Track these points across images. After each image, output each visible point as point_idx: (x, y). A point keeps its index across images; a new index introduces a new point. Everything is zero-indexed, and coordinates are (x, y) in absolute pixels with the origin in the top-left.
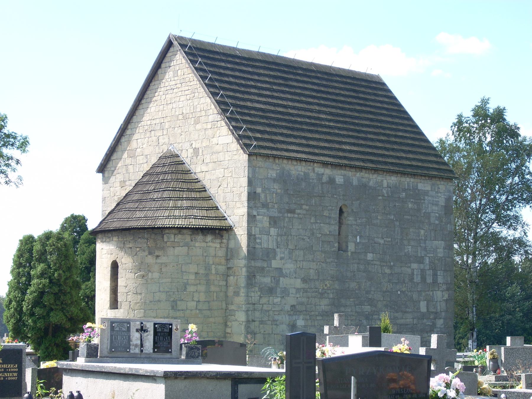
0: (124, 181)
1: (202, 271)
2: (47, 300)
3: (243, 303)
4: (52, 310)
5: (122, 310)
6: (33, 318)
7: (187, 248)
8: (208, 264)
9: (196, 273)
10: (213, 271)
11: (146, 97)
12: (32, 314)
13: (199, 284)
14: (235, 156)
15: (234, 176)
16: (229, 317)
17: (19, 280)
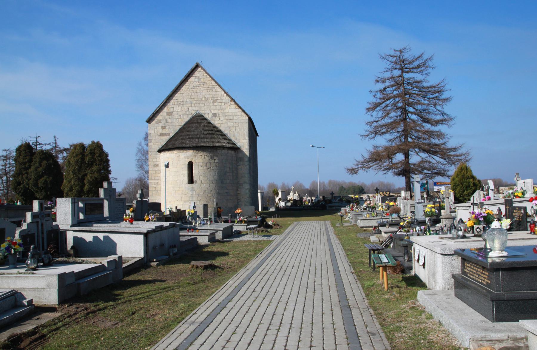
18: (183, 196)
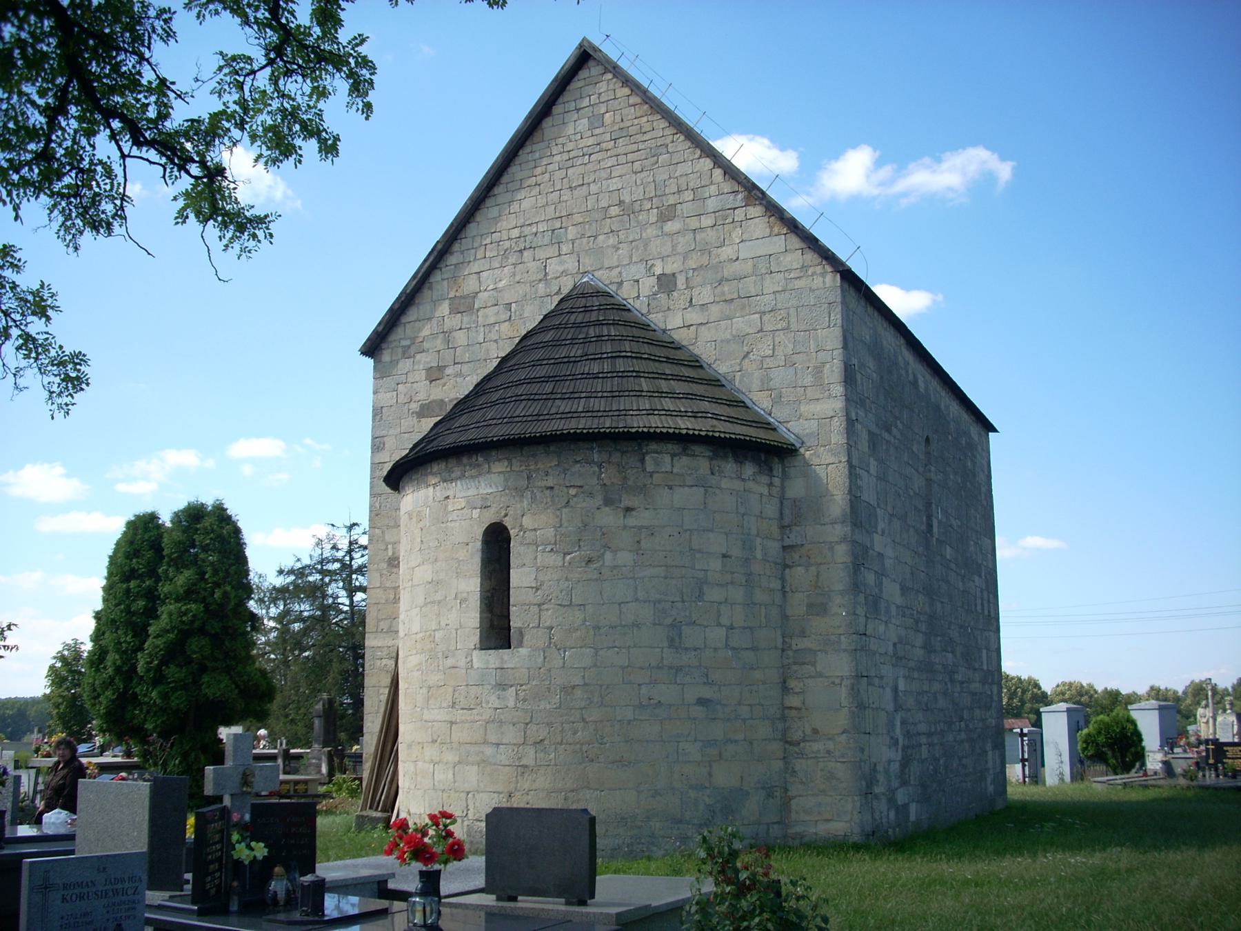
0: (441, 368)
1: (736, 552)
2: (197, 647)
3: (841, 631)
4: (203, 669)
5: (523, 651)
6: (161, 688)
7: (702, 489)
8: (749, 534)
9: (724, 556)
10: (759, 555)
11: (505, 179)
12: (158, 679)
13: (732, 583)
14: (796, 282)
15: (794, 326)
16: (795, 667)
17: (128, 606)
18: (459, 715)
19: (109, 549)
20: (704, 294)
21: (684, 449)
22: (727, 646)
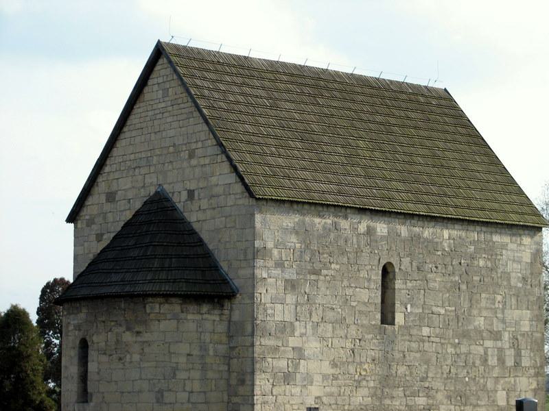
1: (196, 352)
9: (188, 355)
10: (211, 353)
13: (193, 369)
19: (39, 297)
20: (204, 204)
21: (166, 301)
22: (189, 401)
